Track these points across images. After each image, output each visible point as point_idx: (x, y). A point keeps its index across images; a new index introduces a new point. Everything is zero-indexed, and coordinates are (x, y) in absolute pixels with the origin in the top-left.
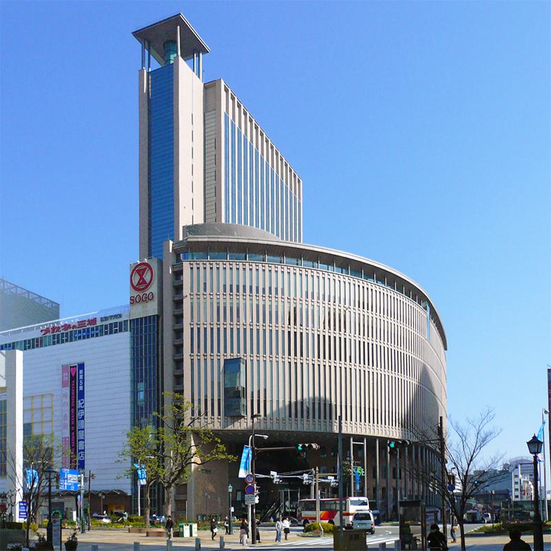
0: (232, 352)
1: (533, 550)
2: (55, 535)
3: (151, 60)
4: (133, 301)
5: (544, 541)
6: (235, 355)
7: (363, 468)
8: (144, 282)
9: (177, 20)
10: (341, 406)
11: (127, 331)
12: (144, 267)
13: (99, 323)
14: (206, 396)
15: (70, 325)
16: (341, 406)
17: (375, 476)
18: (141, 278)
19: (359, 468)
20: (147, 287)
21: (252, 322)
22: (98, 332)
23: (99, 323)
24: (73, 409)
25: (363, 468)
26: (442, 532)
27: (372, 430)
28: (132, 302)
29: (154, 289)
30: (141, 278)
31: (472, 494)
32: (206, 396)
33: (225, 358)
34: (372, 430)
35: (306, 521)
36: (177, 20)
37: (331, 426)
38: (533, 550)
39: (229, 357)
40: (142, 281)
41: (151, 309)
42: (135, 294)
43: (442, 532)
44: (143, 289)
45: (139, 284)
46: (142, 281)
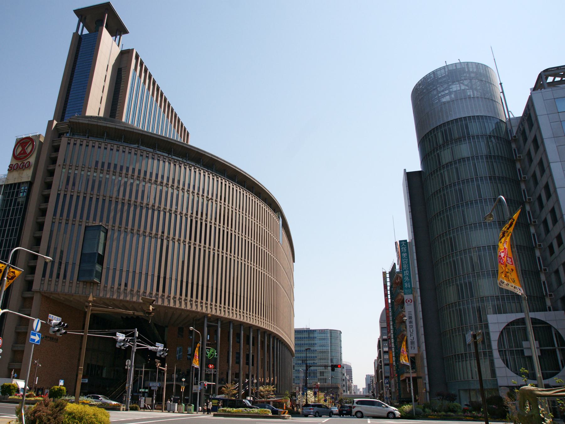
0: (94, 219)
1: (564, 348)
3: (171, 126)
4: (11, 168)
6: (97, 223)
8: (25, 153)
9: (108, 5)
10: (212, 287)
12: (28, 140)
16: (212, 287)
17: (238, 363)
18: (23, 149)
20: (25, 157)
21: (87, 191)
25: (216, 349)
27: (238, 316)
28: (10, 169)
29: (32, 160)
30: (23, 149)
33: (87, 225)
34: (238, 316)
35: (52, 410)
36: (108, 5)
37: (97, 250)
38: (564, 348)
39: (90, 224)
40: (24, 152)
41: (26, 175)
42: (15, 162)
44: (23, 158)
45: (20, 154)
46: (24, 152)
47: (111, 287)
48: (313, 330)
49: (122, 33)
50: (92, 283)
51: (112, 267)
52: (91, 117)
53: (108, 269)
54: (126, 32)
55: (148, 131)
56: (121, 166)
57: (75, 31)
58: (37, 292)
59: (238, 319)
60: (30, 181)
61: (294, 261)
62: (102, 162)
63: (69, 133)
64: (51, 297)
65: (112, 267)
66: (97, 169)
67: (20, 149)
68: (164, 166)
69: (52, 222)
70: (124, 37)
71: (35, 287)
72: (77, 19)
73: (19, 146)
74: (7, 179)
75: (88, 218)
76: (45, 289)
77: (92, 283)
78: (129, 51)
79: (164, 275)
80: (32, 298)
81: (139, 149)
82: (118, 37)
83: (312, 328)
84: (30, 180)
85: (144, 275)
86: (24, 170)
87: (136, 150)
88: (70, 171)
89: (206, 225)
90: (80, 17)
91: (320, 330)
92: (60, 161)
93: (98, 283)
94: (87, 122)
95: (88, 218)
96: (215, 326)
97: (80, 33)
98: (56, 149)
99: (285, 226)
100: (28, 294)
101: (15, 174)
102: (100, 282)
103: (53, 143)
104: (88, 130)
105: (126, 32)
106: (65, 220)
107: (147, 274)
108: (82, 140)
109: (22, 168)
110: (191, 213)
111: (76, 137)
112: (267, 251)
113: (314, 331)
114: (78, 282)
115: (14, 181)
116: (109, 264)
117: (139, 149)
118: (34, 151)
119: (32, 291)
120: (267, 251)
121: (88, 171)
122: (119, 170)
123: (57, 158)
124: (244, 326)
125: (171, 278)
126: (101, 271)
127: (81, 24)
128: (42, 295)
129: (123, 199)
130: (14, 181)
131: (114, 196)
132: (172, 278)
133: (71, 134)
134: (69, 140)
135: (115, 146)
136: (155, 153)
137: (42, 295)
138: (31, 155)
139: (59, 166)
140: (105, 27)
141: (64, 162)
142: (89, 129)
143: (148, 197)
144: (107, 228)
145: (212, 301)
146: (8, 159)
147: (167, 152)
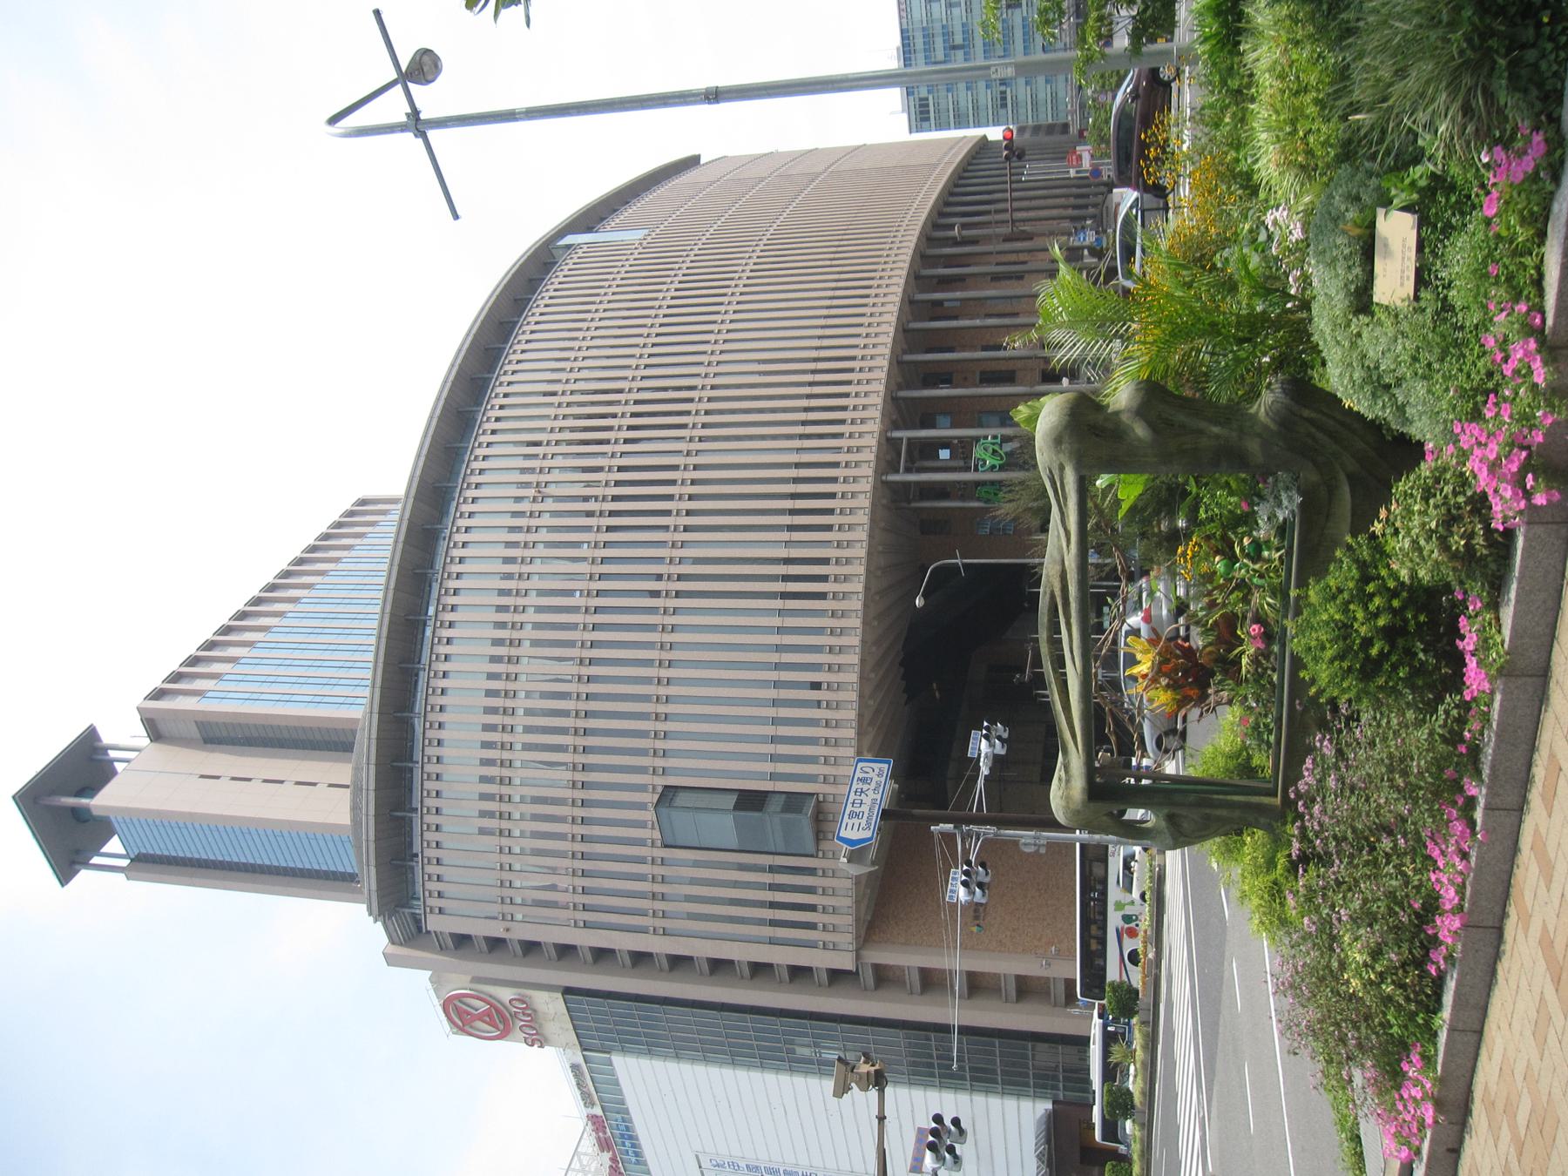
2: (1409, 248)
4: (537, 1038)
5: (1375, 299)
7: (977, 439)
8: (487, 1013)
11: (610, 1059)
13: (598, 1111)
14: (760, 922)
15: (611, 1167)
19: (978, 452)
20: (497, 1010)
21: (572, 659)
22: (620, 1119)
23: (598, 1111)
24: (1093, 620)
26: (93, 861)
29: (506, 994)
30: (480, 1018)
31: (1560, 1033)
32: (760, 922)
33: (659, 843)
40: (487, 1017)
41: (551, 1005)
43: (93, 861)
47: (824, 783)
48: (903, 39)
49: (99, 744)
50: (817, 817)
51: (769, 767)
52: (355, 808)
53: (774, 777)
54: (90, 736)
55: (364, 701)
56: (485, 713)
57: (122, 876)
58: (858, 957)
59: (883, 375)
60: (563, 995)
61: (692, 162)
62: (480, 782)
63: (413, 911)
64: (869, 918)
65: (769, 767)
66: (506, 692)
67: (480, 1024)
68: (467, 591)
69: (664, 934)
70: (107, 738)
71: (845, 962)
72: (84, 876)
73: (471, 1027)
74: (566, 1046)
75: (640, 842)
76: (849, 938)
77: (817, 817)
78: (146, 719)
79: (779, 564)
80: (877, 968)
81: (430, 666)
82: (113, 754)
83: (897, 41)
84: (560, 995)
85: (784, 637)
86: (535, 1011)
87: (432, 674)
88: (517, 850)
89: (615, 498)
90: (77, 867)
91: (901, 17)
92: (496, 930)
93: (818, 802)
94: (373, 870)
95: (640, 842)
96: (909, 451)
97: (125, 863)
98: (462, 941)
99: (591, 218)
100: (868, 976)
101: (551, 1028)
102: (813, 794)
103: (447, 948)
104: (395, 862)
105: (90, 736)
106: (655, 902)
107: (779, 648)
108: (426, 877)
109: (529, 1015)
110: (596, 501)
111: (417, 848)
112: (677, 279)
113: (905, 35)
114: (820, 854)
115: (567, 1030)
116: (760, 776)
117: (430, 666)
118: (482, 992)
119: (857, 969)
120: (677, 279)
121: (512, 920)
122: (493, 768)
123: (487, 939)
124: (908, 322)
125: (794, 496)
126: (784, 796)
127: (96, 860)
128: (866, 941)
129: (577, 715)
130: (567, 1030)
131: (568, 775)
132: (798, 449)
133: (415, 903)
134: (431, 912)
135: (428, 785)
136: (436, 620)
137: (866, 941)
138: (491, 996)
139: (508, 930)
140: (92, 796)
141: (496, 918)
142: (393, 860)
143: (552, 784)
144: (660, 790)
145: (838, 450)
146: (513, 1050)
147: (421, 628)
